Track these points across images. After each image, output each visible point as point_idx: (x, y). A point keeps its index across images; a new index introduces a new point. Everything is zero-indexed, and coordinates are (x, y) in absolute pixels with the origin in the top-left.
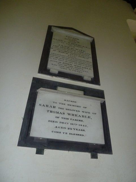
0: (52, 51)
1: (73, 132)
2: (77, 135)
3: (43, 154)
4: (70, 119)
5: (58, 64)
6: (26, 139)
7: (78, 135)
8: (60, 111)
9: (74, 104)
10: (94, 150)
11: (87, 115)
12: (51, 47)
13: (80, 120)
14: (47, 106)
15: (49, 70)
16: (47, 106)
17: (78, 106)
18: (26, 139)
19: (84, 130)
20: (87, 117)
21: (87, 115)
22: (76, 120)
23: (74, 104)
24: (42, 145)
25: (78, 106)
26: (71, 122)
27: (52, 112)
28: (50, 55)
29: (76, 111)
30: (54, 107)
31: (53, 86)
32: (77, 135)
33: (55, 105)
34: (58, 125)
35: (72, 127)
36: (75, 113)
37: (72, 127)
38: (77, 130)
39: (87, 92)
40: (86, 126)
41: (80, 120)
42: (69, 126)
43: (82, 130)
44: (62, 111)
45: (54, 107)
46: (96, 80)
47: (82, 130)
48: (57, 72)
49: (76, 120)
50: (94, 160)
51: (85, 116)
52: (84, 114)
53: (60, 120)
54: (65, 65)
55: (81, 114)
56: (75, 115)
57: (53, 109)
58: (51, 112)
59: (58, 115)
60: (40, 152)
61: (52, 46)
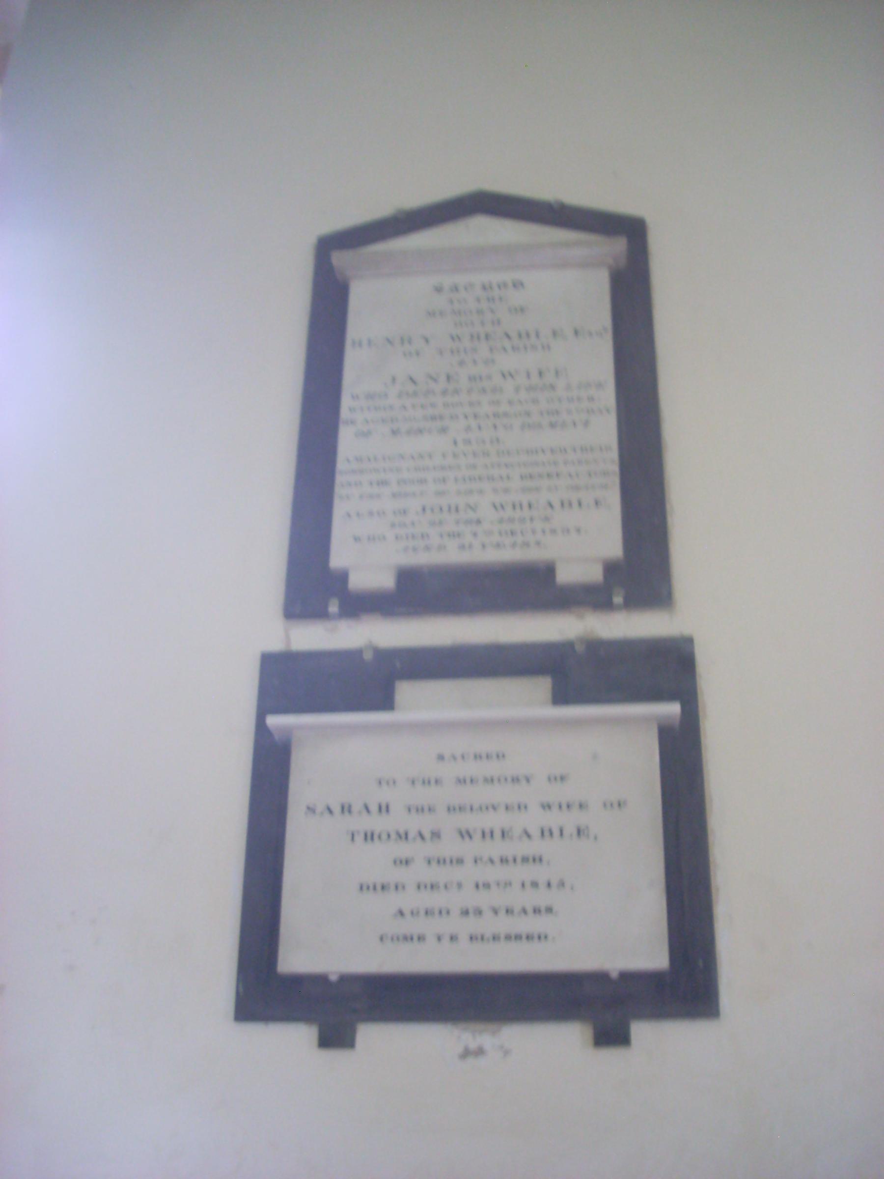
0: (348, 443)
1: (489, 925)
2: (508, 937)
3: (689, 641)
4: (469, 861)
5: (393, 525)
6: (266, 989)
7: (518, 937)
8: (413, 823)
9: (492, 768)
10: (605, 1006)
11: (570, 820)
12: (344, 413)
13: (525, 860)
14: (346, 809)
15: (343, 577)
16: (346, 809)
17: (516, 780)
18: (266, 989)
19: (549, 910)
20: (570, 829)
21: (570, 820)
22: (504, 860)
23: (492, 768)
24: (338, 1008)
25: (516, 780)
26: (518, 822)
27: (376, 837)
28: (339, 479)
29: (502, 809)
30: (384, 809)
31: (367, 684)
32: (508, 937)
33: (385, 795)
34: (410, 900)
35: (484, 899)
36: (495, 821)
37: (484, 899)
38: (509, 911)
39: (581, 676)
40: (562, 884)
41: (525, 860)
42: (470, 898)
43: (537, 911)
44: (426, 823)
45: (384, 809)
46: (643, 568)
47: (537, 911)
48: (386, 581)
49: (504, 860)
50: (611, 1056)
51: (556, 832)
52: (553, 819)
53: (420, 872)
54: (433, 524)
55: (534, 819)
56: (498, 834)
57: (377, 823)
58: (369, 837)
59: (404, 850)
60: (336, 1037)
61: (346, 402)
